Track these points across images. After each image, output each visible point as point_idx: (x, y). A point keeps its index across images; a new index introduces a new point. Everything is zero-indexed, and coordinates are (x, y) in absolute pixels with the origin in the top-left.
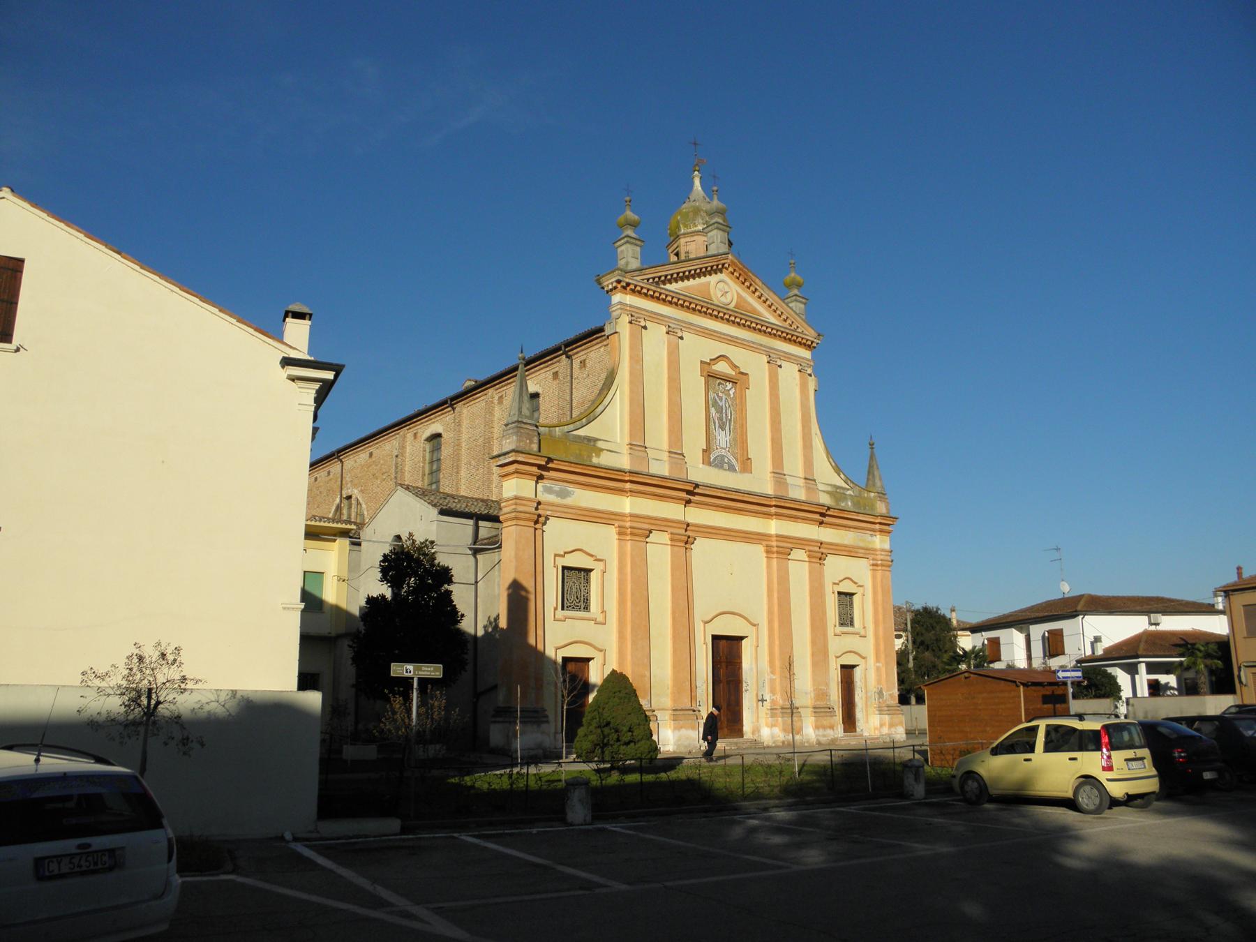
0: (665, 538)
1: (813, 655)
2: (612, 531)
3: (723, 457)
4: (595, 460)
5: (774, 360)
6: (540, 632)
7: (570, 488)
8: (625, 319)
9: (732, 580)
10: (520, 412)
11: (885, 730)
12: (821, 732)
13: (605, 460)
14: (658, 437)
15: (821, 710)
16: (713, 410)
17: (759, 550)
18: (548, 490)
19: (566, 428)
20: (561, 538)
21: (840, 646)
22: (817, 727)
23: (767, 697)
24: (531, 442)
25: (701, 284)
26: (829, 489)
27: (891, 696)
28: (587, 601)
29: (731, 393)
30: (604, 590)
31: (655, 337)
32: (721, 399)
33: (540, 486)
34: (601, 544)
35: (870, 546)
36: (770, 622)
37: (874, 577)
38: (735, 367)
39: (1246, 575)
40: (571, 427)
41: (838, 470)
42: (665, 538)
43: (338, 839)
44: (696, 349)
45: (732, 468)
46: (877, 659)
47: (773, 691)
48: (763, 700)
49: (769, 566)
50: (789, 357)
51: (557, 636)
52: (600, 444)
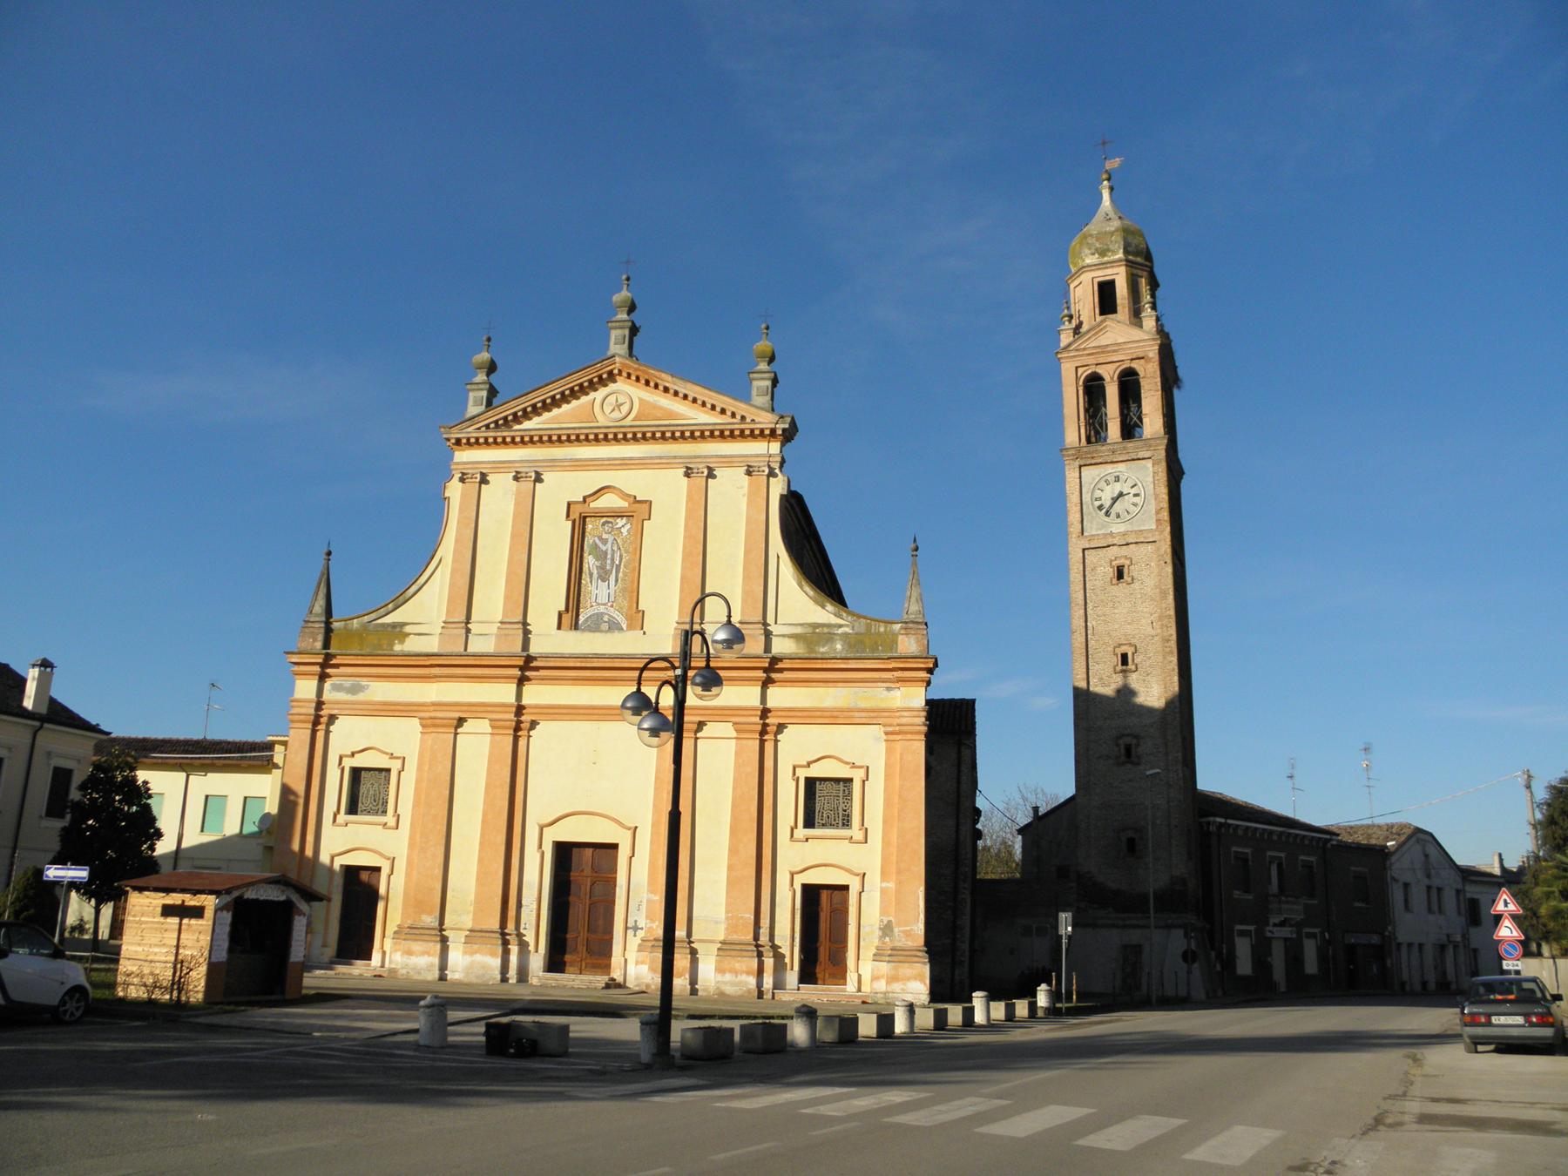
0: (484, 726)
1: (730, 868)
4: (397, 648)
6: (310, 838)
7: (364, 682)
9: (596, 777)
10: (692, 623)
11: (881, 986)
12: (728, 977)
13: (412, 645)
14: (491, 603)
15: (760, 947)
16: (590, 561)
18: (336, 688)
19: (366, 619)
20: (352, 739)
21: (806, 857)
22: (720, 970)
24: (315, 640)
25: (582, 405)
26: (799, 630)
27: (908, 934)
28: (385, 803)
29: (624, 530)
30: (405, 793)
31: (500, 496)
32: (605, 542)
33: (328, 685)
35: (883, 705)
37: (889, 752)
38: (624, 495)
40: (373, 616)
42: (727, 729)
43: (755, 1018)
45: (614, 627)
46: (884, 875)
47: (649, 917)
48: (636, 928)
50: (729, 461)
52: (408, 629)
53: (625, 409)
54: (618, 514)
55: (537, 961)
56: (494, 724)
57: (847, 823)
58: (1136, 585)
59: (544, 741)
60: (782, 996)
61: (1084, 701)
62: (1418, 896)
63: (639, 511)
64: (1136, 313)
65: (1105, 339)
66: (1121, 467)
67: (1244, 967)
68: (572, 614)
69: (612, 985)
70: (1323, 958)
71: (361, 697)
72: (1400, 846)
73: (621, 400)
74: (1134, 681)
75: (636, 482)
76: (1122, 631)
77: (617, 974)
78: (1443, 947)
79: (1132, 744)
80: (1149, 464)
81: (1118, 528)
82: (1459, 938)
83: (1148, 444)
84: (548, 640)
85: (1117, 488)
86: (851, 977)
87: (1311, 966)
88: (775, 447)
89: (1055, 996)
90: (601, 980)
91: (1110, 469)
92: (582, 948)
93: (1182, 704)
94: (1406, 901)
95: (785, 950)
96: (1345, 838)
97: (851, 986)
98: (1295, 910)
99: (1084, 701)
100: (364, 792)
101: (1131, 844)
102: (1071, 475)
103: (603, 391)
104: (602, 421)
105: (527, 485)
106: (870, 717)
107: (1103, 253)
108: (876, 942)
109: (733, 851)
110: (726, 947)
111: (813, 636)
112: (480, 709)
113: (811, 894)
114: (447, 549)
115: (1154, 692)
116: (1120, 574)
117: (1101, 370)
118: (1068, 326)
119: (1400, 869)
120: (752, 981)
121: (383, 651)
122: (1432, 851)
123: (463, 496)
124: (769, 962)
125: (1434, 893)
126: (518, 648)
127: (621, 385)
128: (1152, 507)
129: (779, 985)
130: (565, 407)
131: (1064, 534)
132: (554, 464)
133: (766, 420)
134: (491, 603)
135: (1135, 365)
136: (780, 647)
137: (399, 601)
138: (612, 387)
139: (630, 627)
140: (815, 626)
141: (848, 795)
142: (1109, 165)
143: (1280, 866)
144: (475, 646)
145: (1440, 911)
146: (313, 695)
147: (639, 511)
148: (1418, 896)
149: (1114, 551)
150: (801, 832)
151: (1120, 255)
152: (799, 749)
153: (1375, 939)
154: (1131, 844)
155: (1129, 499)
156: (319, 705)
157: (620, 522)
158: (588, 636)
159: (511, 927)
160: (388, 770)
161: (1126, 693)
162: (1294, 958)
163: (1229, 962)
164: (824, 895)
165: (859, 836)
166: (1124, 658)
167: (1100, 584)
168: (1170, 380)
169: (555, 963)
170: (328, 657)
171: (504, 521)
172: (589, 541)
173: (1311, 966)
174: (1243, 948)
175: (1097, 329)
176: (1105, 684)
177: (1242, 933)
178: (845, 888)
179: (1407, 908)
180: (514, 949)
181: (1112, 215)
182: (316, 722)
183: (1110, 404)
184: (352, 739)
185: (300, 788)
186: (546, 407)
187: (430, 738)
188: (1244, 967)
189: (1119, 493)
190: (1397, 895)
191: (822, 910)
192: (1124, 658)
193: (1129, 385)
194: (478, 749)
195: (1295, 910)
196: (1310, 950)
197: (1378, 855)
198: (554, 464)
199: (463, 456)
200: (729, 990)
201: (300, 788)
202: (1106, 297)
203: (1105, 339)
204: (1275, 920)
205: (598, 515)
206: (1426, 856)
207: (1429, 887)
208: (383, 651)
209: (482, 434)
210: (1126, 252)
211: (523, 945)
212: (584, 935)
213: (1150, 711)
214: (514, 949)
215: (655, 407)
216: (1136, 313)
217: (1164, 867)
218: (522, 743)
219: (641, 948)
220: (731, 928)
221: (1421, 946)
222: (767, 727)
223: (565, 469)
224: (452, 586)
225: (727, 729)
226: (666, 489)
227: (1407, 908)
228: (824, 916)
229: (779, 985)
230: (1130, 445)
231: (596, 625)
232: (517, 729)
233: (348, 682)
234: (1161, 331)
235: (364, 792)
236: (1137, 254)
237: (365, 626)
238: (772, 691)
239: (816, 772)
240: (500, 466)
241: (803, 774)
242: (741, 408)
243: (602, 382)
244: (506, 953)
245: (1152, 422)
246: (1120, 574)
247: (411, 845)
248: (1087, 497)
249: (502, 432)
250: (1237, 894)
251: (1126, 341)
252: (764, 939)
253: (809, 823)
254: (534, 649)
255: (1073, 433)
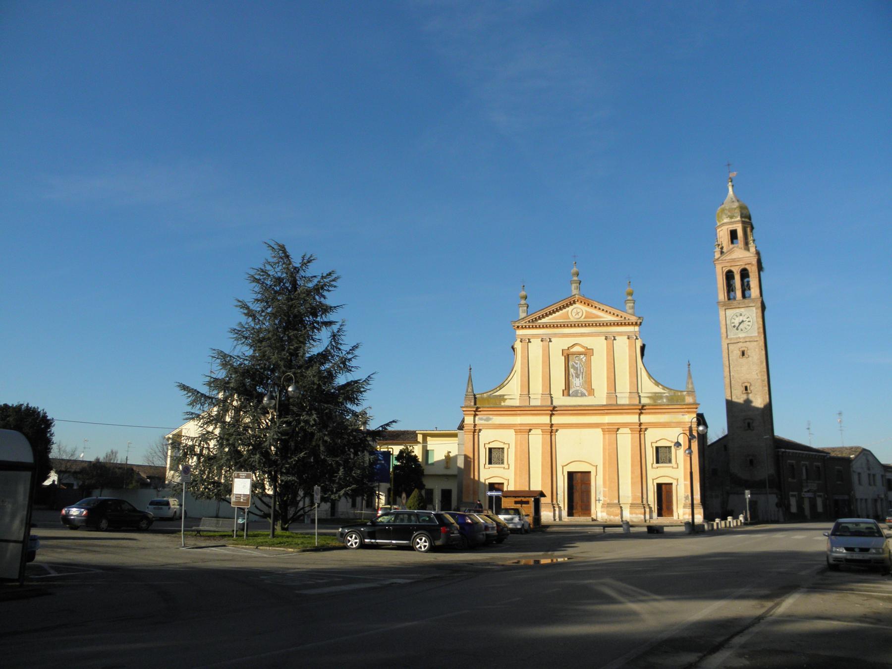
0: (539, 431)
1: (632, 478)
2: (512, 431)
3: (577, 391)
4: (503, 404)
5: (610, 339)
6: (476, 473)
8: (519, 340)
9: (581, 448)
12: (634, 515)
13: (508, 403)
14: (537, 387)
15: (644, 505)
16: (572, 371)
17: (599, 431)
20: (487, 438)
21: (657, 474)
22: (631, 513)
23: (602, 498)
28: (503, 460)
30: (511, 456)
31: (536, 348)
33: (477, 418)
34: (504, 438)
36: (604, 464)
38: (583, 347)
39: (129, 462)
41: (657, 384)
42: (627, 430)
44: (559, 345)
45: (583, 395)
47: (604, 496)
49: (604, 438)
51: (487, 474)
53: (580, 314)
54: (580, 354)
55: (565, 513)
56: (543, 431)
57: (670, 461)
58: (750, 359)
59: (561, 436)
60: (652, 521)
61: (730, 404)
62: (865, 478)
63: (588, 352)
64: (746, 244)
65: (734, 256)
66: (742, 310)
67: (794, 509)
68: (567, 390)
69: (593, 520)
70: (825, 505)
71: (490, 422)
72: (856, 457)
73: (577, 311)
74: (751, 397)
75: (587, 342)
76: (745, 379)
77: (594, 516)
78: (875, 501)
79: (749, 420)
80: (754, 309)
81: (742, 335)
82: (883, 496)
83: (754, 300)
84: (560, 400)
85: (741, 319)
86: (675, 514)
87: (820, 509)
88: (637, 328)
89: (746, 518)
90: (589, 519)
91: (738, 311)
92: (579, 507)
93: (769, 407)
94: (859, 480)
95: (652, 506)
96: (833, 454)
97: (675, 517)
98: (813, 486)
99: (730, 404)
100: (495, 456)
101: (751, 462)
102: (722, 313)
103: (571, 308)
104: (572, 319)
105: (546, 343)
106: (678, 424)
107: (731, 217)
108: (683, 502)
109: (633, 472)
110: (633, 506)
111: (655, 397)
112: (537, 426)
113: (659, 486)
114: (518, 366)
115: (759, 402)
116: (743, 354)
117: (733, 269)
118: (718, 250)
119: (856, 467)
120: (642, 517)
121: (496, 405)
122: (870, 458)
123: (522, 347)
124: (647, 510)
125: (872, 477)
126: (549, 403)
127: (577, 305)
128: (756, 326)
129: (651, 517)
130: (557, 314)
131: (721, 338)
132: (555, 335)
133: (633, 319)
134: (537, 387)
135: (747, 267)
136: (644, 401)
137: (501, 387)
138: (574, 306)
139: (589, 395)
140: (656, 393)
141: (670, 452)
142: (731, 175)
143: (807, 470)
144: (533, 403)
145: (875, 485)
146: (472, 422)
147: (588, 352)
148: (865, 478)
149: (740, 345)
150: (655, 465)
151: (739, 218)
152: (654, 437)
153: (846, 497)
154: (751, 462)
155: (746, 323)
156: (475, 425)
157: (582, 356)
158: (574, 398)
159: (555, 502)
160: (503, 449)
161: (748, 402)
162: (813, 506)
163: (788, 507)
164: (663, 486)
165: (675, 466)
166: (746, 388)
167: (736, 359)
168: (760, 268)
169: (570, 514)
170: (477, 408)
171: (537, 359)
172: (571, 363)
173: (820, 509)
174: (793, 502)
175: (730, 251)
176: (739, 398)
177: (793, 496)
178: (671, 484)
179: (860, 483)
180: (557, 509)
181: (734, 199)
182: (474, 432)
183: (736, 283)
184: (487, 438)
185: (471, 456)
186: (547, 315)
187: (519, 437)
188: (794, 509)
189: (744, 319)
190: (855, 478)
191: (664, 492)
192: (746, 388)
193: (744, 274)
194: (537, 439)
195: (813, 486)
196: (819, 501)
197: (846, 461)
198: (555, 335)
199: (520, 332)
200: (635, 520)
201: (471, 456)
202: (733, 235)
203: (734, 256)
204: (805, 490)
205: (573, 354)
206: (868, 461)
207: (869, 475)
208: (496, 405)
209: (527, 324)
210: (742, 217)
211: (560, 508)
212: (580, 503)
213: (757, 409)
214: (557, 509)
215: (591, 313)
216: (746, 244)
217: (766, 471)
218: (553, 437)
219: (602, 507)
220: (634, 498)
221: (866, 500)
222: (641, 429)
223: (560, 337)
224: (522, 381)
225: (627, 430)
226: (598, 344)
227: (860, 483)
228: (664, 493)
229: (651, 517)
230: (746, 301)
231: (576, 394)
232: (551, 432)
233: (485, 417)
234: (758, 253)
235: (495, 456)
236: (745, 217)
237: (489, 397)
238: (642, 416)
239: (659, 444)
240: (535, 336)
241: (655, 445)
242: (624, 315)
243: (571, 304)
244: (554, 510)
245: (754, 292)
246: (743, 354)
247: (515, 474)
248: (728, 322)
249: (533, 323)
250: (790, 480)
251: (741, 257)
252: (645, 502)
253: (657, 462)
254: (555, 404)
255: (722, 295)
